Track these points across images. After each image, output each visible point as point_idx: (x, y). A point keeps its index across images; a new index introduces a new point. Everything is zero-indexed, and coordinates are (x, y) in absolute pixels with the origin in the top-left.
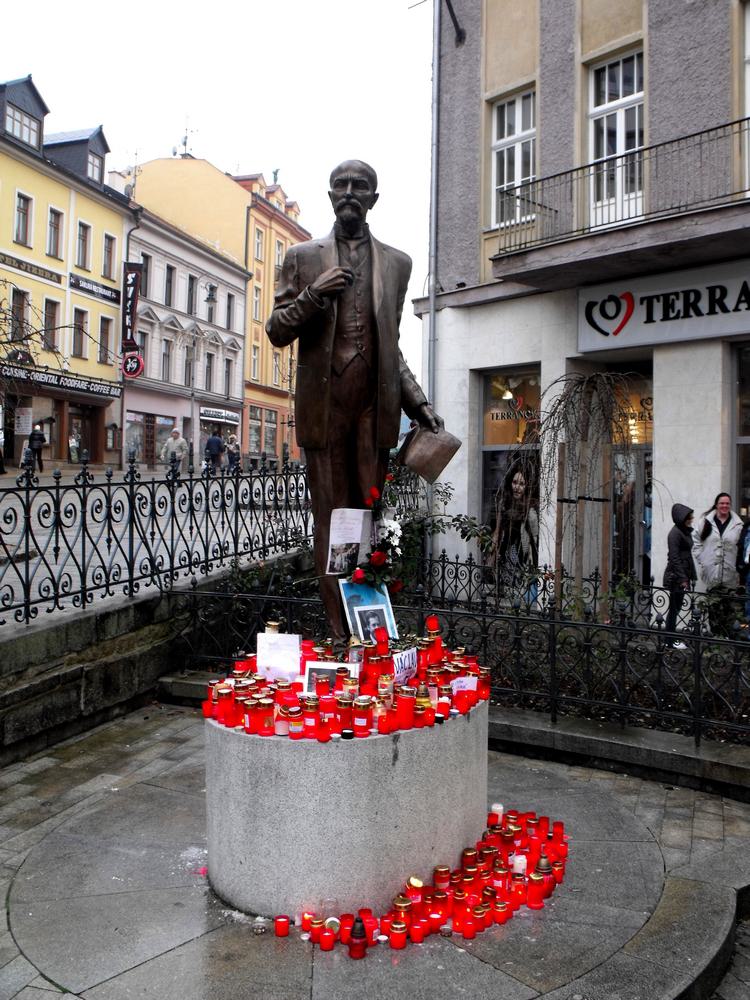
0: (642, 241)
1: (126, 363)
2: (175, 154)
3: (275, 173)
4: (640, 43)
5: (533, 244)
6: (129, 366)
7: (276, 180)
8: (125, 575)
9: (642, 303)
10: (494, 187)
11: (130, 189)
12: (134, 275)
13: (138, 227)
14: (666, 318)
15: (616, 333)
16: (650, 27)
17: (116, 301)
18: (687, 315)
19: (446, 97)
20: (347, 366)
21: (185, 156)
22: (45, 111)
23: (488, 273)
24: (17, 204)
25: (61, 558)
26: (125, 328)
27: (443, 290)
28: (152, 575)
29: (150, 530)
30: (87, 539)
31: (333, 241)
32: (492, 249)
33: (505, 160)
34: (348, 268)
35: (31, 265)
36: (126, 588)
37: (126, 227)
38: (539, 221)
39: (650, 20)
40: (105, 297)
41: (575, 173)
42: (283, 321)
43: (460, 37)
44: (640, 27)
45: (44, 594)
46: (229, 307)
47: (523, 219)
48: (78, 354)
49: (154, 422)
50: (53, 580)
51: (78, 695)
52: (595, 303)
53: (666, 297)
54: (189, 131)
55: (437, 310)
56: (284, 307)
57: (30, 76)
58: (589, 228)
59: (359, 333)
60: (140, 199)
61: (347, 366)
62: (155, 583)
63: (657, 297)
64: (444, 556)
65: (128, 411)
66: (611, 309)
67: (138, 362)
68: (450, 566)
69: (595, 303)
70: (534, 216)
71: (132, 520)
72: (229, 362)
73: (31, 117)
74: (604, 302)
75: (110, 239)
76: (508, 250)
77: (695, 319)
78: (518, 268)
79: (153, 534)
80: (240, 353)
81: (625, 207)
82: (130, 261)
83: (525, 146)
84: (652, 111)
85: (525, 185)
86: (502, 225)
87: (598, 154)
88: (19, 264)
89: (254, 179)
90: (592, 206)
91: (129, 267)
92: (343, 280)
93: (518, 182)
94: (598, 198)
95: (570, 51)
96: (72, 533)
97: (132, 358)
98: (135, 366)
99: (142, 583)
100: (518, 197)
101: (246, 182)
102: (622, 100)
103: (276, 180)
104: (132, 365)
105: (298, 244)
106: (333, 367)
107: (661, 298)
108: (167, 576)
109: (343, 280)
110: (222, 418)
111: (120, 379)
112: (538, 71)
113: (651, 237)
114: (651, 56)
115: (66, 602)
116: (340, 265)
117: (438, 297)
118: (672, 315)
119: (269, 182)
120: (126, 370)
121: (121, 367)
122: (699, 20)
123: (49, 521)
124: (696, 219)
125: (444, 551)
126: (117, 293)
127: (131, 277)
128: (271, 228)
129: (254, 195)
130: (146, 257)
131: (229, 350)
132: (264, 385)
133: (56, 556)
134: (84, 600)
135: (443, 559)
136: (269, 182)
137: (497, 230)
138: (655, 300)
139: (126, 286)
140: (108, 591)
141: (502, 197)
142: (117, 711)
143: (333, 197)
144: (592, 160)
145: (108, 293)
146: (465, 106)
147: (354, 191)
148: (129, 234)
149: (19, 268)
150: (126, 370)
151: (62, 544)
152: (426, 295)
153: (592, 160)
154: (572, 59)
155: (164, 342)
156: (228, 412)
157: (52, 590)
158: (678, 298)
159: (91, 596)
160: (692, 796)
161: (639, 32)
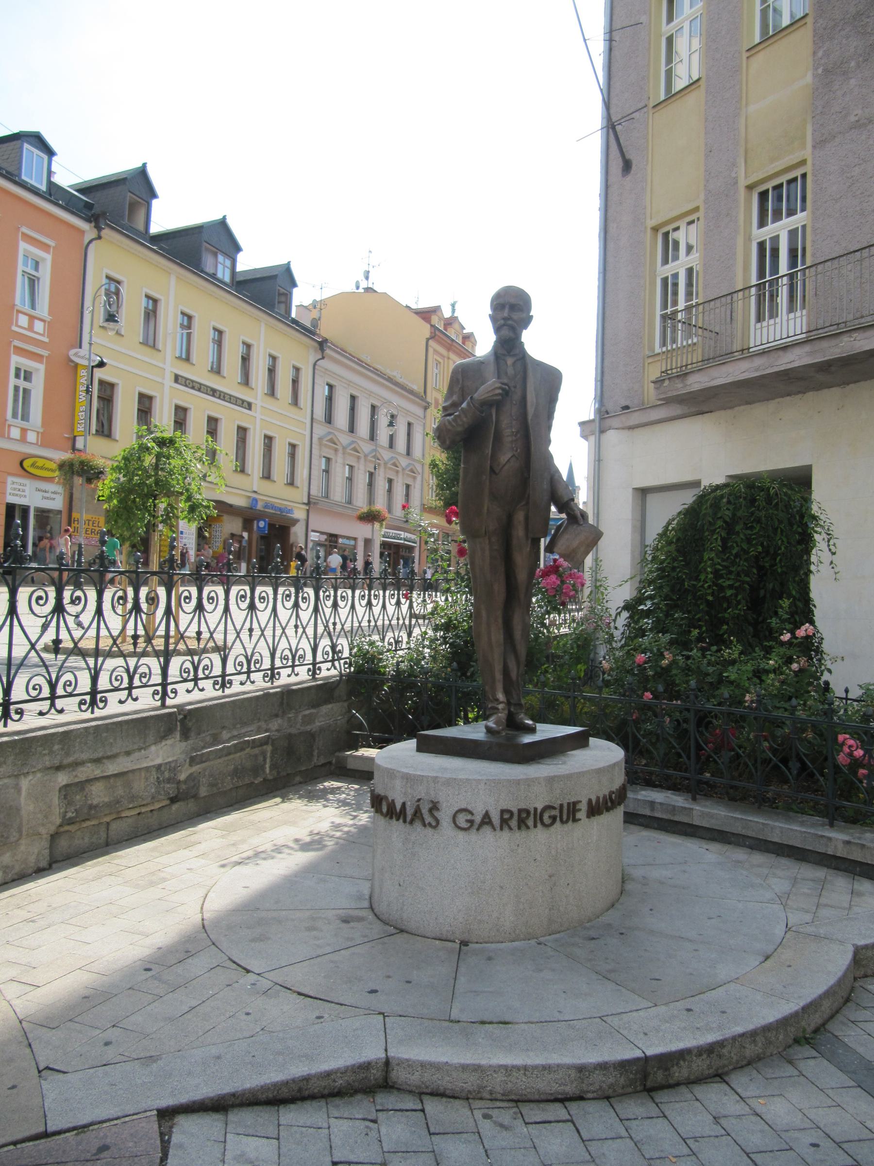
0: (797, 359)
2: (358, 288)
3: (453, 306)
4: (803, 162)
5: (694, 365)
7: (453, 311)
8: (309, 657)
10: (658, 313)
11: (315, 322)
13: (323, 358)
16: (814, 147)
19: (612, 227)
20: (504, 465)
21: (368, 290)
22: (238, 249)
23: (651, 393)
24: (212, 336)
25: (255, 638)
27: (608, 413)
28: (333, 661)
29: (332, 620)
30: (277, 622)
31: (492, 359)
32: (654, 372)
33: (669, 286)
34: (505, 381)
35: (225, 393)
36: (309, 670)
37: (313, 356)
38: (700, 342)
39: (814, 139)
41: (735, 295)
42: (449, 427)
43: (627, 166)
44: (803, 146)
45: (239, 668)
46: (409, 434)
48: (267, 476)
49: (336, 542)
50: (246, 657)
51: (265, 760)
54: (371, 267)
55: (602, 431)
56: (450, 415)
57: (224, 217)
58: (749, 349)
59: (514, 438)
60: (325, 331)
61: (504, 465)
62: (335, 668)
65: (313, 531)
70: (695, 340)
71: (316, 610)
72: (408, 487)
73: (226, 255)
76: (669, 372)
78: (679, 388)
79: (334, 624)
80: (419, 478)
81: (789, 324)
83: (690, 271)
84: (814, 230)
85: (688, 309)
86: (664, 349)
87: (761, 274)
88: (214, 392)
89: (436, 310)
92: (500, 391)
93: (682, 305)
94: (759, 319)
95: (733, 175)
96: (264, 616)
99: (324, 666)
100: (679, 321)
101: (426, 314)
102: (785, 221)
103: (453, 311)
105: (459, 361)
106: (491, 468)
108: (345, 663)
109: (500, 391)
110: (401, 539)
112: (702, 197)
113: (810, 354)
114: (814, 175)
115: (257, 677)
116: (499, 378)
117: (602, 419)
119: (447, 314)
122: (864, 137)
123: (244, 605)
124: (855, 335)
128: (449, 358)
129: (432, 326)
131: (408, 475)
133: (251, 636)
134: (273, 676)
136: (447, 314)
137: (659, 354)
140: (293, 671)
141: (665, 322)
142: (298, 779)
143: (493, 318)
144: (754, 282)
146: (630, 231)
147: (511, 311)
148: (315, 365)
149: (213, 396)
151: (255, 625)
152: (592, 417)
153: (754, 282)
154: (736, 183)
156: (406, 534)
157: (245, 666)
159: (20, 712)
160: (821, 873)
161: (802, 153)
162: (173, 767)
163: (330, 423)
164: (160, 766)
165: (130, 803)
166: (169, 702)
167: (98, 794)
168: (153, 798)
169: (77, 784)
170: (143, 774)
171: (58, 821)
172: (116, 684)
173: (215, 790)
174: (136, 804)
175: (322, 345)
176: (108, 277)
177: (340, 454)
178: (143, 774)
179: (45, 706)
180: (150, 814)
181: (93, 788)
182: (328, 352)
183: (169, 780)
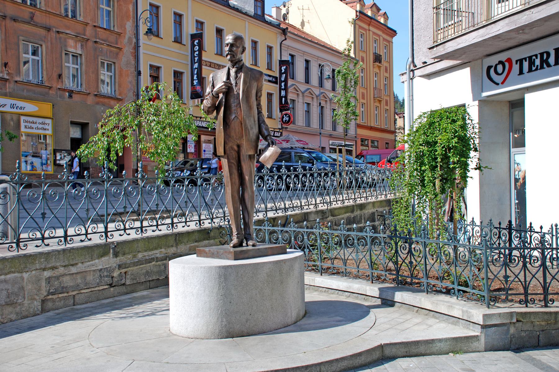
1: (283, 117)
6: (284, 119)
9: (516, 63)
12: (285, 67)
14: (530, 70)
15: (503, 83)
17: (276, 83)
18: (542, 67)
26: (281, 98)
37: (281, 38)
40: (269, 81)
47: (446, 25)
52: (492, 66)
53: (530, 58)
63: (525, 59)
64: (473, 221)
66: (500, 68)
67: (289, 117)
68: (536, 235)
69: (492, 66)
74: (496, 65)
75: (270, 48)
77: (547, 69)
82: (283, 59)
90: (496, 6)
91: (282, 63)
97: (286, 115)
98: (288, 119)
104: (286, 118)
107: (528, 59)
111: (280, 127)
118: (534, 68)
120: (283, 121)
121: (280, 120)
125: (531, 224)
126: (276, 78)
127: (283, 68)
128: (369, 30)
130: (292, 56)
132: (369, 125)
135: (531, 229)
138: (524, 60)
139: (281, 74)
145: (271, 79)
148: (281, 44)
150: (283, 121)
155: (305, 105)
158: (537, 58)
159: (26, 245)
162: (110, 270)
163: (308, 83)
164: (101, 269)
165: (85, 286)
166: (109, 240)
167: (67, 281)
168: (98, 284)
169: (55, 277)
170: (92, 273)
171: (45, 294)
172: (78, 232)
173: (135, 282)
174: (88, 287)
175: (284, 32)
176: (151, 5)
177: (301, 97)
178: (92, 273)
179: (210, 221)
180: (98, 292)
181: (64, 279)
182: (289, 34)
183: (107, 276)
